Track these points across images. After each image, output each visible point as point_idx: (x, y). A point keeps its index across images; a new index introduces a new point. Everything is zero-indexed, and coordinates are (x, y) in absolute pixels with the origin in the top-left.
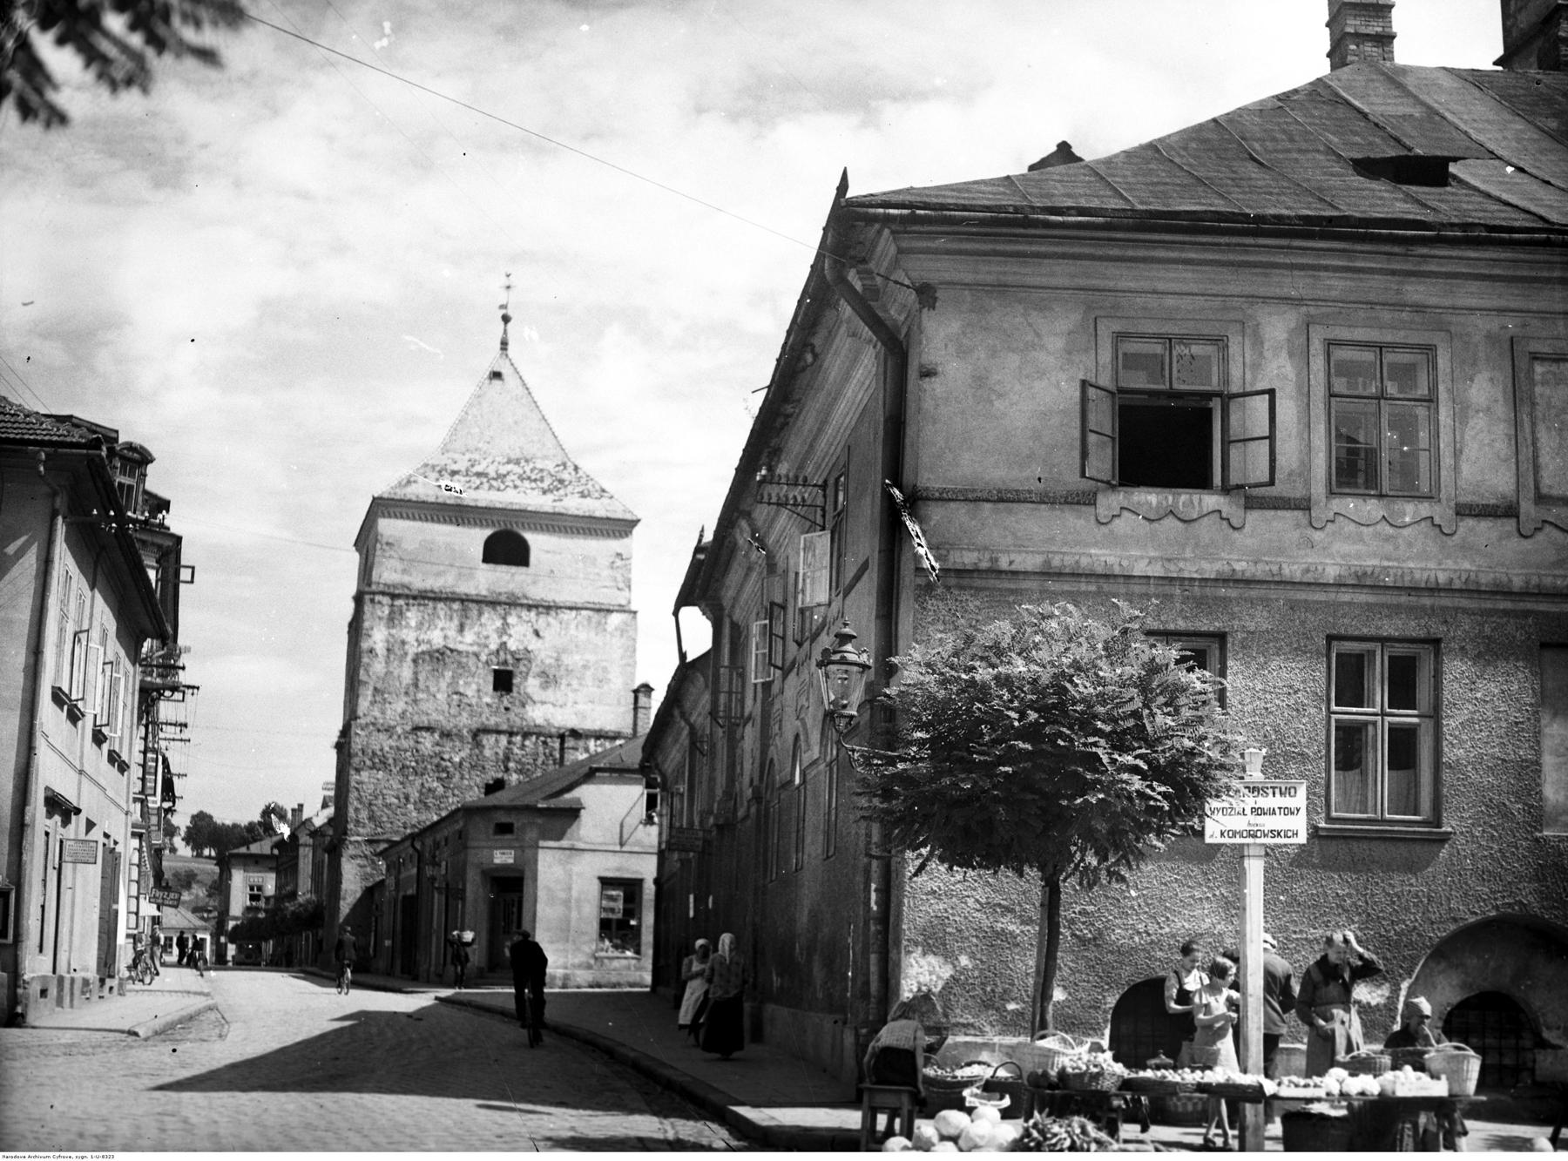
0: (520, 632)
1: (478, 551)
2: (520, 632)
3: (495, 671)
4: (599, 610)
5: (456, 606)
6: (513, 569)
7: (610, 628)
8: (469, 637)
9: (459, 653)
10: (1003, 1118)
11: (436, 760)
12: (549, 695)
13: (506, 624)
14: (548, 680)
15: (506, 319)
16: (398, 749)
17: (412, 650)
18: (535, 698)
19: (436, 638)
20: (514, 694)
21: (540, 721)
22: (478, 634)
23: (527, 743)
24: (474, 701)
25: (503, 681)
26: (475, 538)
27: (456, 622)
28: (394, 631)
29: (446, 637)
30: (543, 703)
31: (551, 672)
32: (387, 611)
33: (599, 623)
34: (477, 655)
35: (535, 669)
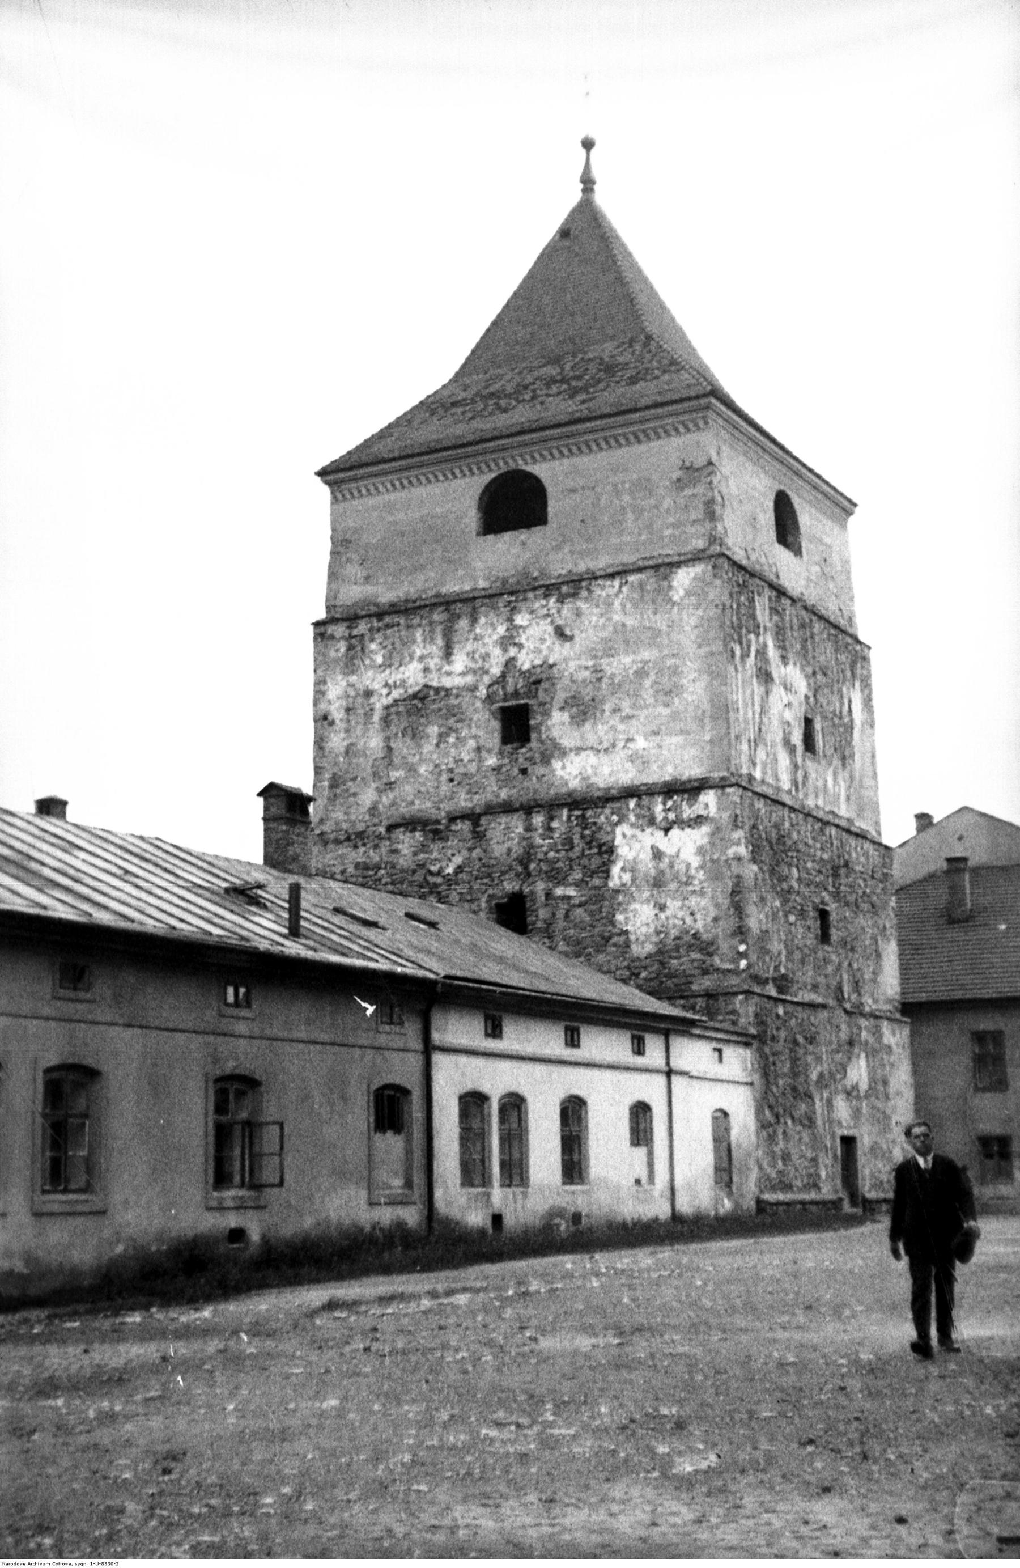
0: (535, 640)
1: (472, 518)
2: (535, 640)
3: (504, 710)
4: (656, 567)
5: (438, 616)
6: (523, 535)
7: (677, 594)
8: (460, 662)
9: (448, 691)
10: (64, 803)
11: (418, 877)
12: (597, 732)
13: (513, 629)
14: (583, 709)
15: (588, 144)
16: (366, 867)
17: (379, 703)
18: (566, 742)
19: (412, 675)
20: (534, 744)
21: (574, 784)
22: (471, 655)
23: (555, 824)
24: (473, 768)
25: (517, 723)
26: (461, 495)
27: (440, 642)
28: (353, 679)
29: (426, 670)
30: (579, 750)
31: (587, 693)
32: (342, 646)
33: (658, 591)
34: (473, 689)
35: (561, 696)
